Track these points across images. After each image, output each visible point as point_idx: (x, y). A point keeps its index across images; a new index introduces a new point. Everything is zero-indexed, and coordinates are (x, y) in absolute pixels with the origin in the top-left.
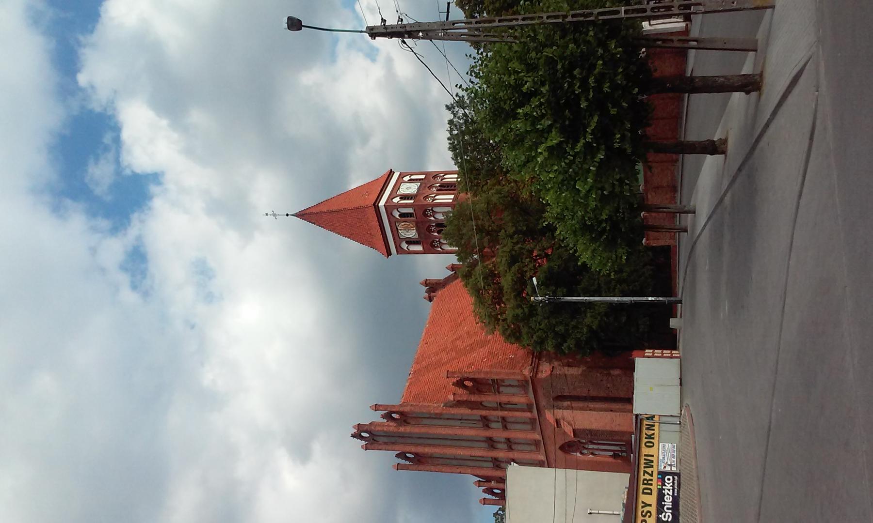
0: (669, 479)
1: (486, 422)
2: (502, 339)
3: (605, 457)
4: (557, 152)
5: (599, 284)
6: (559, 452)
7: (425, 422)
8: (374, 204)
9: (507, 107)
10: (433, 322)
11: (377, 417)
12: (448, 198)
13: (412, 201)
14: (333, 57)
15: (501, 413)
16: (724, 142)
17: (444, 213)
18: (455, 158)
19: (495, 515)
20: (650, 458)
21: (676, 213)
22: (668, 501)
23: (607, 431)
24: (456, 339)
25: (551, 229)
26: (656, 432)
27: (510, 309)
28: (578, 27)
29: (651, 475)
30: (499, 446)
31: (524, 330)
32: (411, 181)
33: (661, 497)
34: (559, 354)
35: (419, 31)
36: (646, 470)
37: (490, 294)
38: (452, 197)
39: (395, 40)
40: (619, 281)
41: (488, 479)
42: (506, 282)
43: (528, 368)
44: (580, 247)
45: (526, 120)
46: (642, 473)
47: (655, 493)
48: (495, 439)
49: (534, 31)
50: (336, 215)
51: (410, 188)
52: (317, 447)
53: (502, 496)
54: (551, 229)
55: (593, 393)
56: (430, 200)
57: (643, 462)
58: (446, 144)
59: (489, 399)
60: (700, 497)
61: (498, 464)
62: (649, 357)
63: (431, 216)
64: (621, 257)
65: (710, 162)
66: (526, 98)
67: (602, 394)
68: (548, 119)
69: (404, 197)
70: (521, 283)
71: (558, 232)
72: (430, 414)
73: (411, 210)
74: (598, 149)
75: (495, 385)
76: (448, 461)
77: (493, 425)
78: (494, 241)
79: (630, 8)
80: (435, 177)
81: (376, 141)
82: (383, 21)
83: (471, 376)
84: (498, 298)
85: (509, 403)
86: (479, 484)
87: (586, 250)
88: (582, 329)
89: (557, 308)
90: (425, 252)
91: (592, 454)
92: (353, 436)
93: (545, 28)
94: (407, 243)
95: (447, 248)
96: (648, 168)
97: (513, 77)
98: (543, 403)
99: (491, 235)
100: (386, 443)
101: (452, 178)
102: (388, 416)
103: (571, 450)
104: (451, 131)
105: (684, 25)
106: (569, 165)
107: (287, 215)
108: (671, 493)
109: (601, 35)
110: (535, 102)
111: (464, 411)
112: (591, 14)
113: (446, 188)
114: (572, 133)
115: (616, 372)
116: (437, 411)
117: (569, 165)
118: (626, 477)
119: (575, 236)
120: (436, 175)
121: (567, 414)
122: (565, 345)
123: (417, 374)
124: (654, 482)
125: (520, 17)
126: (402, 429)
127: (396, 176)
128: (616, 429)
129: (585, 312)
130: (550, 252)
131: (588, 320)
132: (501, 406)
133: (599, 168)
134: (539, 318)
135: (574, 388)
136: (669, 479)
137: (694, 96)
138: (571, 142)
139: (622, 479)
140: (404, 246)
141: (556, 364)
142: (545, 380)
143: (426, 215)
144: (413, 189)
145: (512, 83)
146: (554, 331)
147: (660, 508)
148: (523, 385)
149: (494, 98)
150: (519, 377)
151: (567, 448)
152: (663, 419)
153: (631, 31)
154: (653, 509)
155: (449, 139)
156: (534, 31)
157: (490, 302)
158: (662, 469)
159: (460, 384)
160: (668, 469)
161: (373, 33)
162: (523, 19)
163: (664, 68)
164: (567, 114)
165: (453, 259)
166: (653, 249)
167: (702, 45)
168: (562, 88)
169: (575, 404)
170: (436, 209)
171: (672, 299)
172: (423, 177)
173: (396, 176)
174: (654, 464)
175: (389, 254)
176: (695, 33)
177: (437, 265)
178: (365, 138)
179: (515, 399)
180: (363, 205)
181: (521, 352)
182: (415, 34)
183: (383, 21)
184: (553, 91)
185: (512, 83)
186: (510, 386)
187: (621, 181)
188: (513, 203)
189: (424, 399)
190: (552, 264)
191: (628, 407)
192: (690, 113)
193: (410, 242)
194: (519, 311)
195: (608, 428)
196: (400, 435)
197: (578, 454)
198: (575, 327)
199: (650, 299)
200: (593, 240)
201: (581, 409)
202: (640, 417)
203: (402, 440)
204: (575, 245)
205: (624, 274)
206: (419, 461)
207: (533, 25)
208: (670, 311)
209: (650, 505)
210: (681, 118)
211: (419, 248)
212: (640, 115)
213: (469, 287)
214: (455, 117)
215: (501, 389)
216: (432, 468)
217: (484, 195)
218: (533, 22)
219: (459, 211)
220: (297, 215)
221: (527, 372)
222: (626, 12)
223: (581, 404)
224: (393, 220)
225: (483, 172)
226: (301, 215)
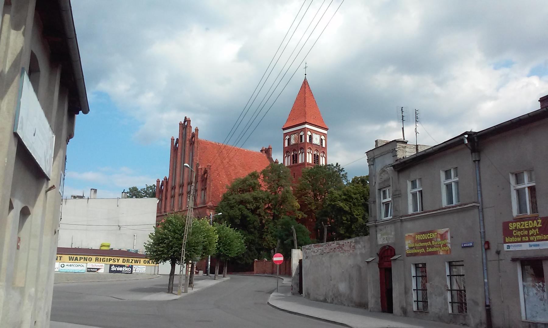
7: (191, 154)
11: (193, 130)
13: (308, 141)
22: (121, 269)
24: (235, 166)
26: (151, 265)
27: (238, 197)
33: (122, 266)
38: (311, 162)
41: (167, 183)
43: (212, 205)
47: (123, 264)
56: (308, 150)
57: (137, 259)
59: (199, 186)
69: (311, 137)
73: (303, 141)
80: (324, 152)
81: (438, 90)
90: (284, 148)
92: (185, 117)
100: (182, 133)
101: (322, 162)
102: (194, 136)
113: (316, 158)
124: (128, 264)
126: (188, 142)
127: (325, 132)
132: (196, 191)
136: (509, 247)
140: (287, 137)
147: (115, 266)
148: (204, 202)
150: (207, 201)
154: (116, 263)
158: (134, 266)
159: (206, 172)
160: (134, 269)
172: (324, 146)
173: (325, 132)
174: (136, 264)
175: (284, 129)
178: (440, 84)
199: (209, 263)
206: (175, 149)
211: (286, 145)
215: (203, 191)
220: (305, 79)
221: (210, 204)
226: (305, 82)
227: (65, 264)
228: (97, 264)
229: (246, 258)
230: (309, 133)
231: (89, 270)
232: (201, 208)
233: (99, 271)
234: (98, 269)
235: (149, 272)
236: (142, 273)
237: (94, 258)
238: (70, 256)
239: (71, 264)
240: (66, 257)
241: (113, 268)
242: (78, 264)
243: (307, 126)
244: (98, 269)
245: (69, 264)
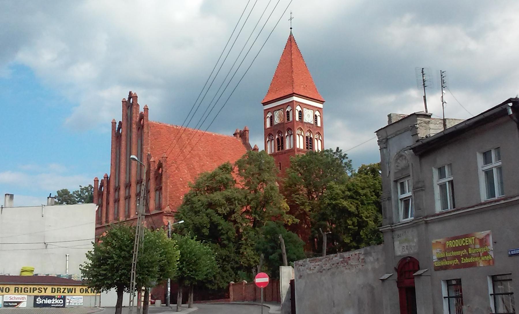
7: (139, 141)
8: (294, 93)
11: (141, 110)
12: (300, 143)
20: (73, 291)
21: (463, 310)
22: (49, 301)
24: (200, 157)
26: (90, 294)
27: (204, 198)
29: (63, 292)
36: (66, 290)
43: (170, 210)
47: (52, 294)
57: (71, 287)
59: (152, 186)
63: (288, 133)
69: (301, 113)
73: (291, 119)
83: (163, 173)
90: (265, 129)
94: (271, 117)
100: (127, 114)
101: (318, 146)
102: (142, 117)
107: (291, 28)
108: (53, 303)
113: (309, 142)
124: (59, 294)
126: (134, 126)
140: (269, 115)
147: (42, 297)
152: (98, 298)
154: (43, 294)
158: (67, 297)
159: (160, 166)
160: (67, 301)
172: (319, 124)
173: (320, 106)
175: (264, 104)
180: (294, 85)
192: (235, 305)
193: (272, 118)
199: (169, 289)
206: (117, 137)
211: (268, 125)
220: (291, 35)
221: (167, 209)
226: (291, 39)
230: (298, 108)
233: (21, 305)
234: (19, 303)
235: (88, 305)
236: (78, 307)
237: (12, 288)
241: (39, 301)
243: (295, 98)
244: (19, 303)
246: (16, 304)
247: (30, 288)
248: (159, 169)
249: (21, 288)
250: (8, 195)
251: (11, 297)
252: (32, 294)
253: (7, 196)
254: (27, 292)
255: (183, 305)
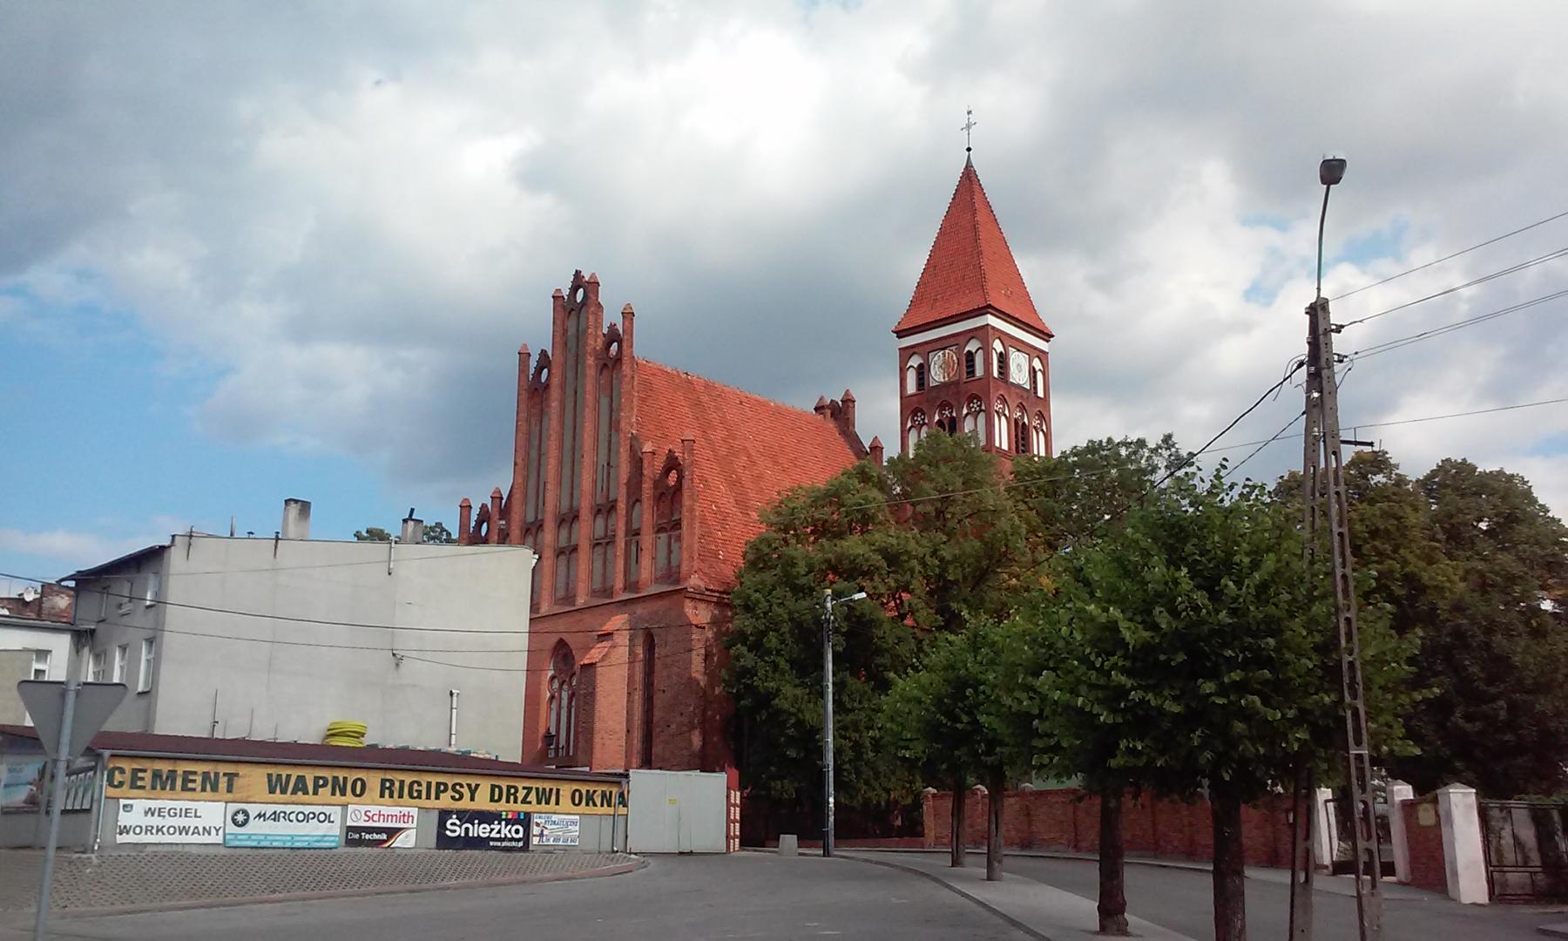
0: (517, 831)
1: (606, 509)
2: (753, 538)
3: (547, 720)
4: (1108, 638)
5: (853, 710)
6: (554, 639)
7: (605, 401)
8: (990, 306)
9: (1189, 548)
10: (779, 413)
11: (611, 316)
12: (1002, 439)
13: (996, 374)
14: (1250, 221)
15: (621, 534)
16: (1123, 931)
17: (975, 430)
18: (1075, 452)
19: (439, 525)
20: (553, 798)
21: (997, 850)
22: (481, 830)
23: (593, 722)
25: (952, 622)
26: (599, 810)
27: (806, 552)
28: (1332, 675)
29: (524, 801)
30: (564, 533)
31: (768, 577)
32: (1033, 372)
33: (487, 817)
34: (728, 640)
35: (1321, 392)
37: (832, 515)
38: (1005, 447)
39: (1303, 350)
40: (857, 746)
41: (505, 512)
42: (854, 545)
44: (924, 676)
45: (1166, 583)
46: (527, 784)
47: (493, 807)
48: (576, 526)
49: (1324, 597)
50: (969, 244)
51: (1019, 372)
52: (546, 201)
53: (474, 539)
54: (952, 622)
55: (659, 700)
56: (998, 406)
57: (547, 785)
58: (1100, 436)
59: (646, 515)
60: (490, 885)
61: (531, 532)
62: (728, 797)
63: (969, 408)
64: (907, 748)
65: (1086, 908)
66: (1210, 585)
67: (657, 714)
68: (1169, 623)
69: (1003, 359)
70: (852, 572)
71: (952, 637)
72: (620, 410)
73: (979, 372)
74: (1114, 711)
75: (670, 526)
76: (536, 443)
77: (600, 521)
78: (924, 523)
79: (1367, 765)
81: (1099, 304)
82: (1339, 329)
83: (686, 484)
84: (823, 530)
85: (639, 549)
86: (496, 497)
87: (922, 688)
88: (773, 679)
89: (809, 636)
91: (552, 697)
92: (578, 273)
93: (1330, 614)
94: (921, 366)
95: (912, 438)
96: (1076, 797)
97: (1247, 560)
98: (640, 610)
99: (936, 519)
100: (565, 331)
101: (1038, 446)
102: (613, 336)
103: (560, 661)
104: (1126, 444)
105: (1327, 861)
106: (1084, 660)
107: (969, 149)
109: (1317, 713)
110: (1200, 597)
111: (624, 470)
112: (1355, 697)
113: (1021, 435)
114: (1145, 663)
115: (697, 740)
116: (623, 424)
117: (1084, 660)
118: (515, 756)
119: (945, 669)
120: (1043, 416)
121: (622, 653)
122: (744, 649)
123: (686, 385)
124: (512, 806)
125: (1348, 571)
126: (590, 361)
128: (597, 739)
129: (803, 685)
130: (909, 621)
131: (788, 690)
132: (634, 533)
133: (1080, 711)
134: (790, 603)
135: (666, 666)
136: (517, 831)
137: (1209, 881)
138: (1128, 664)
139: (512, 752)
141: (710, 634)
142: (683, 614)
143: (971, 399)
144: (1018, 375)
145: (1237, 559)
146: (768, 629)
147: (467, 816)
149: (1202, 525)
150: (684, 568)
151: (562, 653)
152: (621, 821)
153: (1325, 766)
154: (465, 804)
155: (1110, 440)
156: (1324, 597)
157: (817, 516)
158: (536, 819)
159: (672, 464)
160: (536, 830)
161: (1317, 311)
162: (1344, 576)
163: (1252, 824)
164: (1185, 656)
165: (892, 449)
166: (917, 804)
167: (1299, 895)
168: (1225, 645)
169: (639, 668)
170: (981, 418)
171: (832, 839)
172: (1041, 394)
175: (901, 334)
176: (1321, 882)
177: (881, 418)
178: (1103, 284)
179: (646, 561)
180: (989, 285)
181: (729, 572)
182: (1316, 384)
183: (1339, 329)
184: (1220, 631)
185: (1237, 559)
186: (670, 552)
187: (1056, 749)
188: (995, 557)
189: (643, 400)
190: (887, 626)
191: (635, 760)
193: (922, 372)
194: (802, 568)
195: (598, 725)
196: (579, 358)
197: (551, 673)
198: (775, 667)
199: (831, 800)
200: (939, 701)
201: (631, 678)
202: (624, 781)
203: (571, 362)
204: (925, 667)
205: (871, 754)
206: (534, 391)
207: (1335, 594)
208: (811, 834)
209: (472, 799)
210: (1156, 857)
211: (911, 388)
212: (1174, 782)
213: (844, 479)
214: (1152, 451)
215: (663, 536)
216: (523, 415)
217: (1010, 503)
218: (1340, 595)
219: (974, 462)
220: (969, 166)
221: (695, 581)
222: (1359, 757)
223: (639, 676)
224: (961, 340)
225: (1051, 503)
226: (969, 176)
227: (253, 810)
228: (386, 810)
229: (867, 783)
230: (998, 346)
231: (355, 837)
232: (660, 596)
233: (399, 842)
234: (392, 832)
235: (592, 846)
236: (565, 849)
237: (374, 780)
238: (274, 771)
239: (279, 808)
240: (254, 778)
241: (455, 829)
242: (307, 809)
243: (991, 320)
244: (392, 832)
245: (269, 809)
246: (384, 837)
247: (429, 784)
248: (667, 471)
249: (402, 782)
250: (296, 501)
251: (368, 811)
252: (433, 803)
253: (293, 505)
254: (419, 797)
255: (1386, 879)
